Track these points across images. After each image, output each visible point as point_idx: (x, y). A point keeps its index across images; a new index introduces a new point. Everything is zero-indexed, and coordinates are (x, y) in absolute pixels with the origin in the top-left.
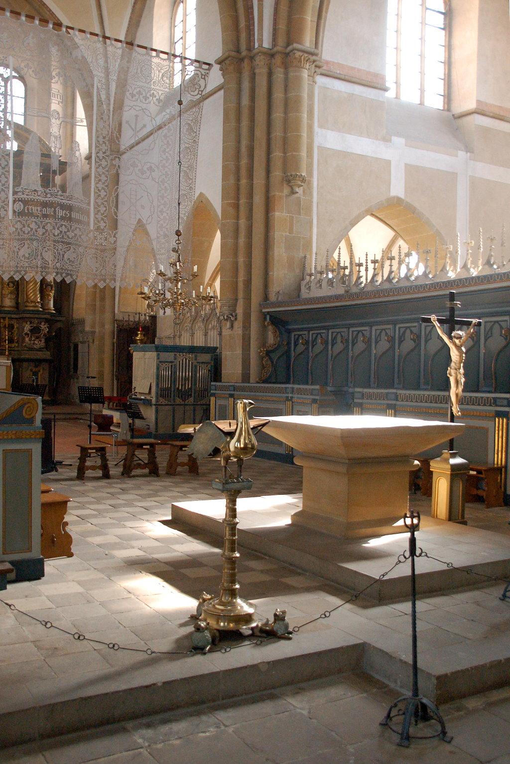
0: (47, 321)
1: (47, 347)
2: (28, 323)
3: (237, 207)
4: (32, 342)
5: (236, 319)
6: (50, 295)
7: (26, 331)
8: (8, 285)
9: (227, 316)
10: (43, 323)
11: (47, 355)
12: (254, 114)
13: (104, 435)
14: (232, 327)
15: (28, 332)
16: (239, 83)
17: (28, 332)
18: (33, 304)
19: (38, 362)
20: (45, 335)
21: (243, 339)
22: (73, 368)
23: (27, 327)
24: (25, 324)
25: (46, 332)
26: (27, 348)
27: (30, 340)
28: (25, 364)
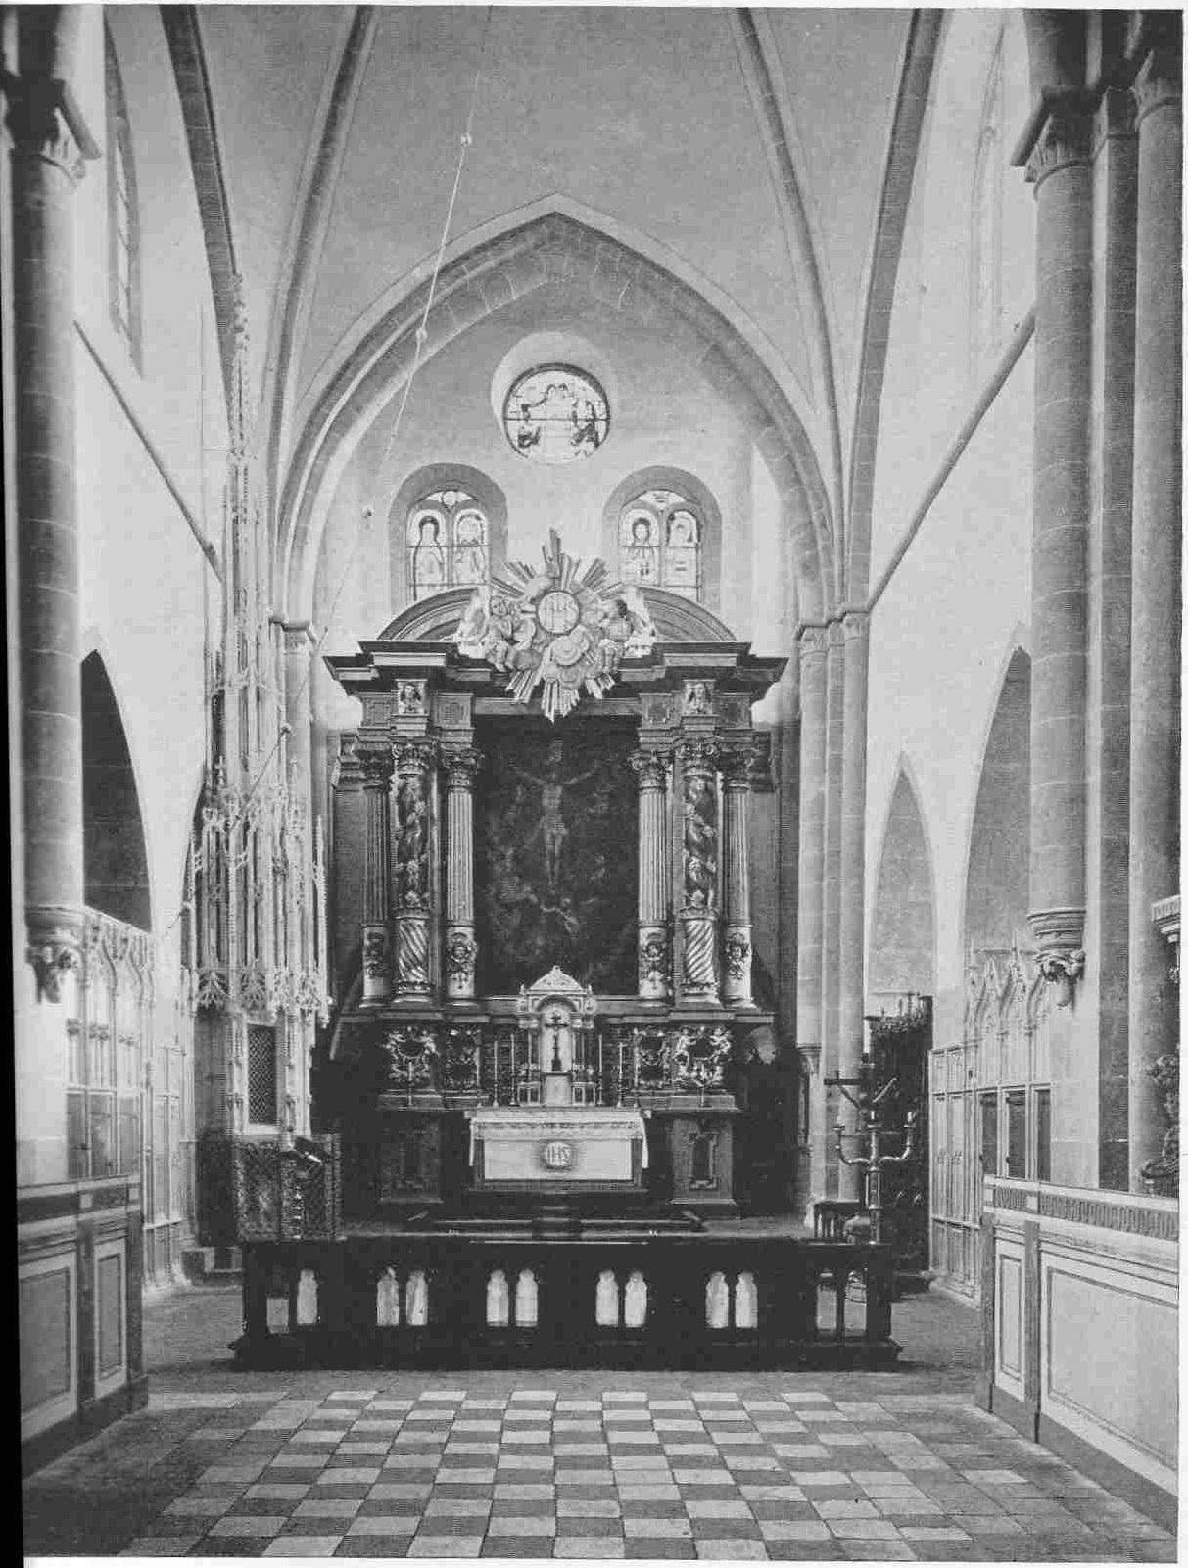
0: (728, 1025)
1: (729, 1084)
2: (685, 1032)
3: (1078, 605)
4: (694, 1074)
5: (1081, 972)
6: (737, 968)
7: (680, 1051)
8: (648, 951)
9: (1052, 963)
10: (718, 1032)
11: (727, 1103)
12: (905, 191)
13: (1049, 1309)
14: (1071, 998)
15: (686, 1053)
16: (1083, 194)
17: (686, 1053)
18: (696, 991)
19: (708, 1121)
20: (723, 1057)
21: (1104, 1034)
22: (1007, 1160)
23: (683, 1042)
24: (677, 1034)
25: (725, 1050)
26: (683, 1087)
27: (690, 1070)
28: (677, 1124)
